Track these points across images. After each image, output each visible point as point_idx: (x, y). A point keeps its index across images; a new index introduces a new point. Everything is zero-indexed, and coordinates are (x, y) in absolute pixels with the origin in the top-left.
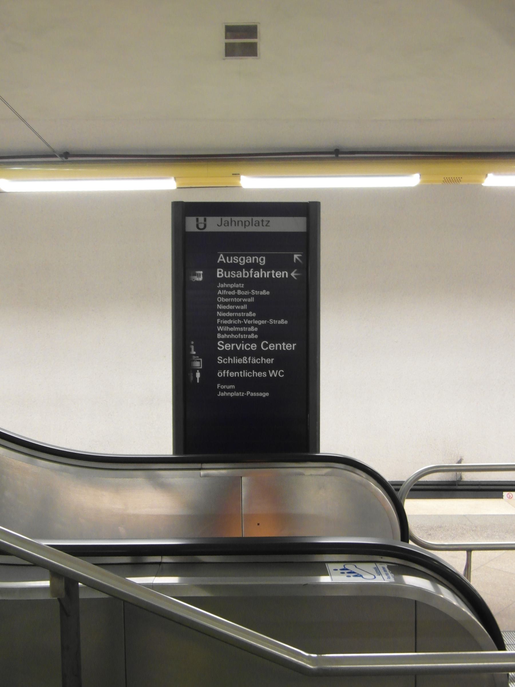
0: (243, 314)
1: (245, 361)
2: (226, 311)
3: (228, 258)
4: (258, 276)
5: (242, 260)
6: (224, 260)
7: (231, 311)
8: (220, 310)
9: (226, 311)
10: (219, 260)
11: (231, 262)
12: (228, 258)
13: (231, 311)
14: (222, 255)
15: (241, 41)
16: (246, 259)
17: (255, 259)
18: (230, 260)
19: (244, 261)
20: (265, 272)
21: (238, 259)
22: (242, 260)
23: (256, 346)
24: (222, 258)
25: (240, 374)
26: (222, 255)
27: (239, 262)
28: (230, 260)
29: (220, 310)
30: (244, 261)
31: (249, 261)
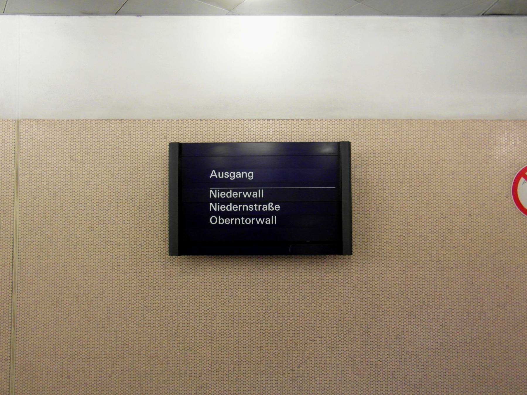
0: (257, 207)
1: (271, 208)
2: (225, 201)
3: (219, 173)
4: (256, 196)
5: (232, 175)
6: (215, 175)
7: (235, 201)
8: (214, 201)
9: (225, 201)
10: (212, 175)
11: (223, 177)
12: (219, 173)
13: (235, 201)
14: (214, 171)
15: (265, 206)
16: (236, 174)
17: (244, 174)
18: (221, 175)
19: (234, 176)
20: (246, 173)
21: (229, 174)
22: (232, 175)
23: (279, 207)
24: (214, 174)
25: (241, 221)
26: (214, 171)
27: (229, 177)
28: (221, 175)
29: (214, 201)
30: (234, 176)
31: (238, 176)
